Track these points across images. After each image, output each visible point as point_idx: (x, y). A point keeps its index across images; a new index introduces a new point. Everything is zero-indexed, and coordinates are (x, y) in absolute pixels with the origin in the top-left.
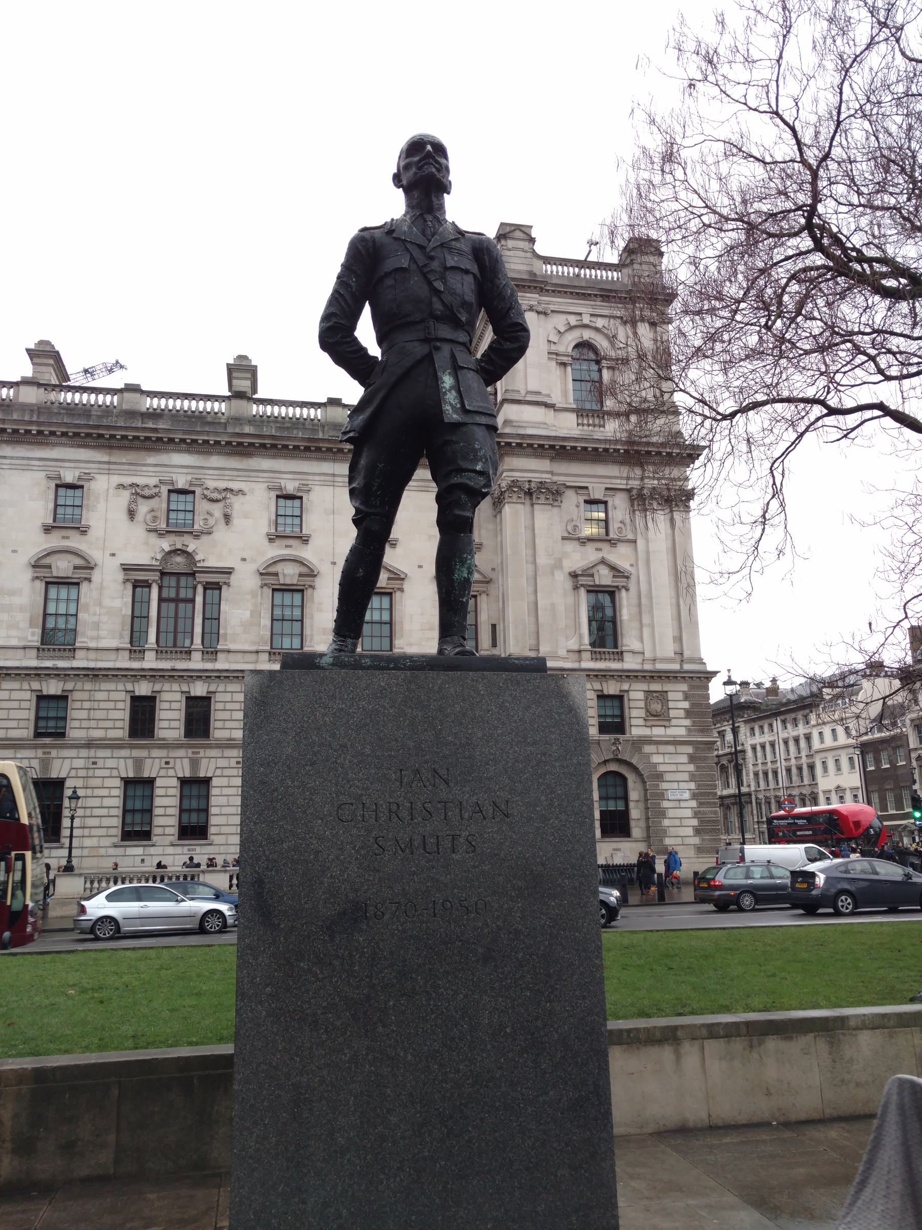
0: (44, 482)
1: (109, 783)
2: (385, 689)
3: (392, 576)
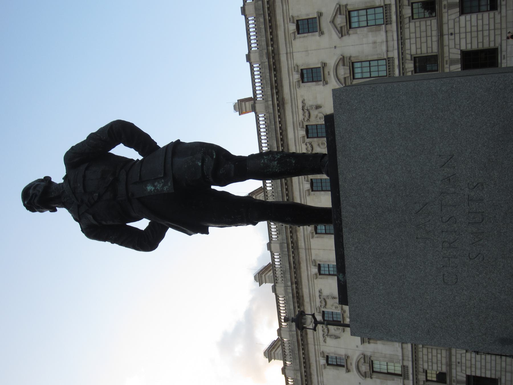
0: (315, 239)
1: (463, 24)
2: (357, 247)
3: (338, 12)
